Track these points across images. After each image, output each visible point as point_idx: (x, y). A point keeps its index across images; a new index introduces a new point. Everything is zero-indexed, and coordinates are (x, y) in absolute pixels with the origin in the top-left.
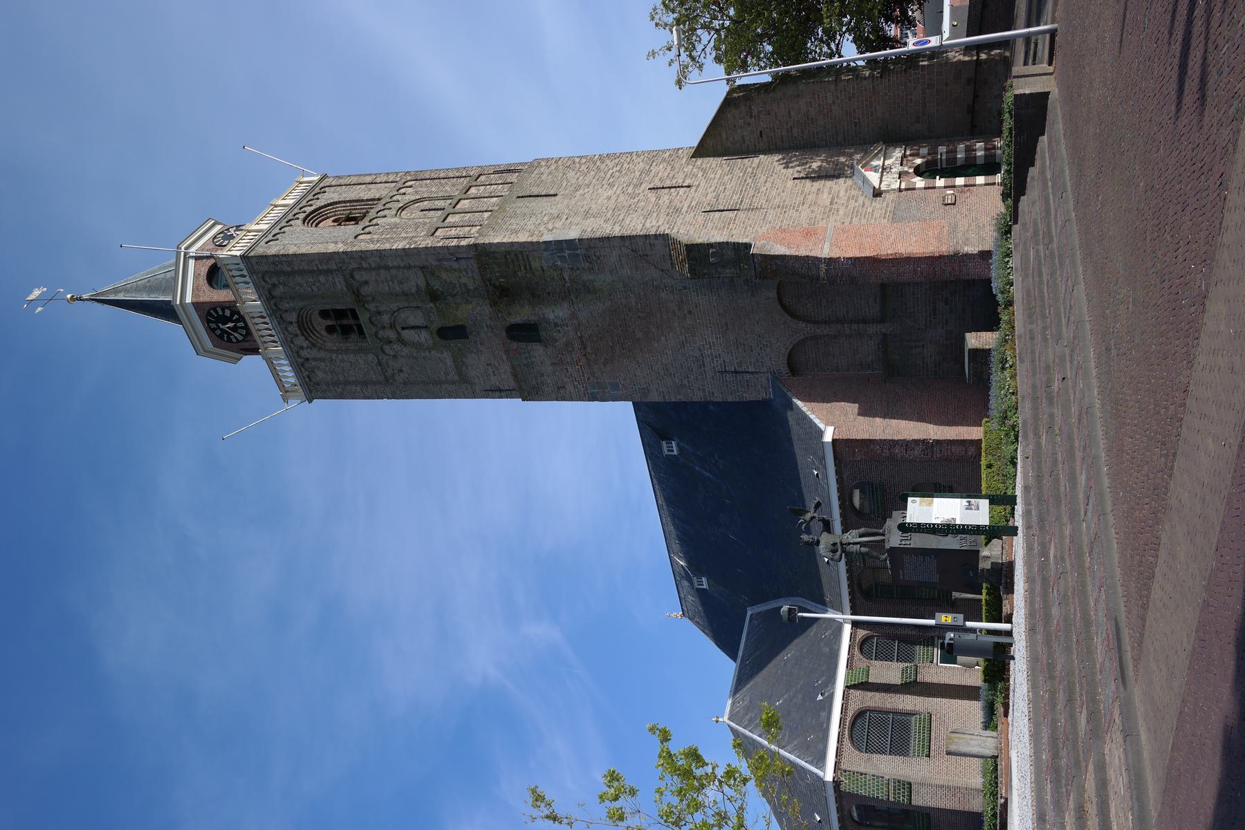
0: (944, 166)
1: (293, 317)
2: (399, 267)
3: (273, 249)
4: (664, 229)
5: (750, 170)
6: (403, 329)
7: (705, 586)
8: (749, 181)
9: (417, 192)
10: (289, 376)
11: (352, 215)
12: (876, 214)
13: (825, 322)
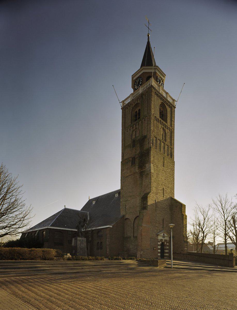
0: (164, 248)
1: (139, 102)
2: (147, 128)
3: (153, 94)
4: (152, 191)
5: (167, 209)
6: (135, 131)
7: (93, 203)
8: (164, 210)
9: (168, 132)
10: (127, 102)
11: (163, 115)
12: (152, 235)
13: (134, 226)
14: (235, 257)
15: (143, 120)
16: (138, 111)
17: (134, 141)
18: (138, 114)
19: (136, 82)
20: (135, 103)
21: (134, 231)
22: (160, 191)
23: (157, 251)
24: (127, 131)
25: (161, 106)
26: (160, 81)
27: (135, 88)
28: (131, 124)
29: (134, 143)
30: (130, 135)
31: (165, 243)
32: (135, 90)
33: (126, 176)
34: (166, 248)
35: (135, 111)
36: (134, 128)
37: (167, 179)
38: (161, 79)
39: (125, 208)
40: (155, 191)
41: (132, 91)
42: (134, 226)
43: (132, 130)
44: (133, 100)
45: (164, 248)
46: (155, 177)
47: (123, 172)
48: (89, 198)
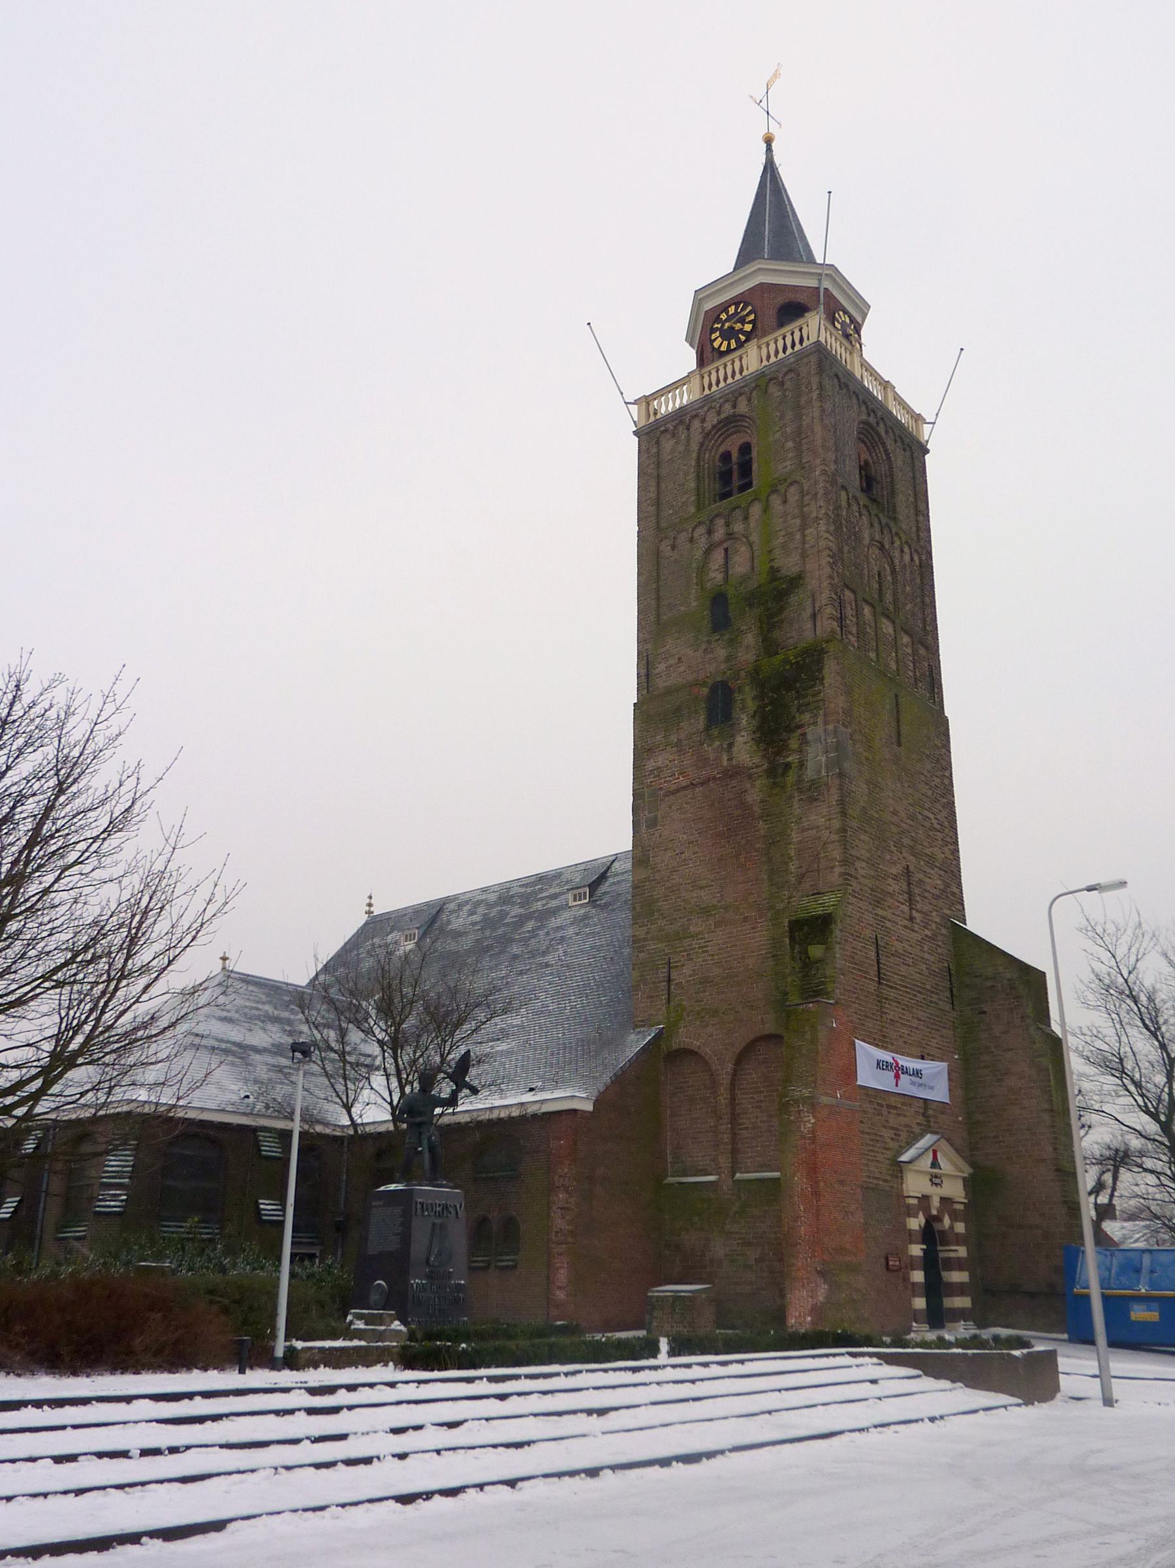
0: (941, 1255)
6: (726, 550)
10: (666, 407)
13: (733, 1099)
14: (560, 1288)
15: (775, 500)
16: (735, 455)
17: (719, 601)
18: (735, 467)
19: (718, 319)
20: (719, 413)
21: (734, 1135)
22: (893, 887)
23: (906, 1279)
24: (673, 548)
25: (863, 442)
26: (852, 332)
27: (713, 348)
28: (699, 509)
29: (720, 612)
30: (694, 565)
31: (947, 1221)
32: (706, 355)
33: (674, 787)
34: (952, 1255)
35: (721, 450)
36: (719, 534)
37: (920, 817)
38: (848, 320)
39: (669, 980)
40: (866, 881)
41: (688, 359)
42: (733, 1099)
43: (703, 543)
44: (707, 401)
45: (941, 1255)
46: (862, 803)
47: (650, 765)
48: (370, 905)
